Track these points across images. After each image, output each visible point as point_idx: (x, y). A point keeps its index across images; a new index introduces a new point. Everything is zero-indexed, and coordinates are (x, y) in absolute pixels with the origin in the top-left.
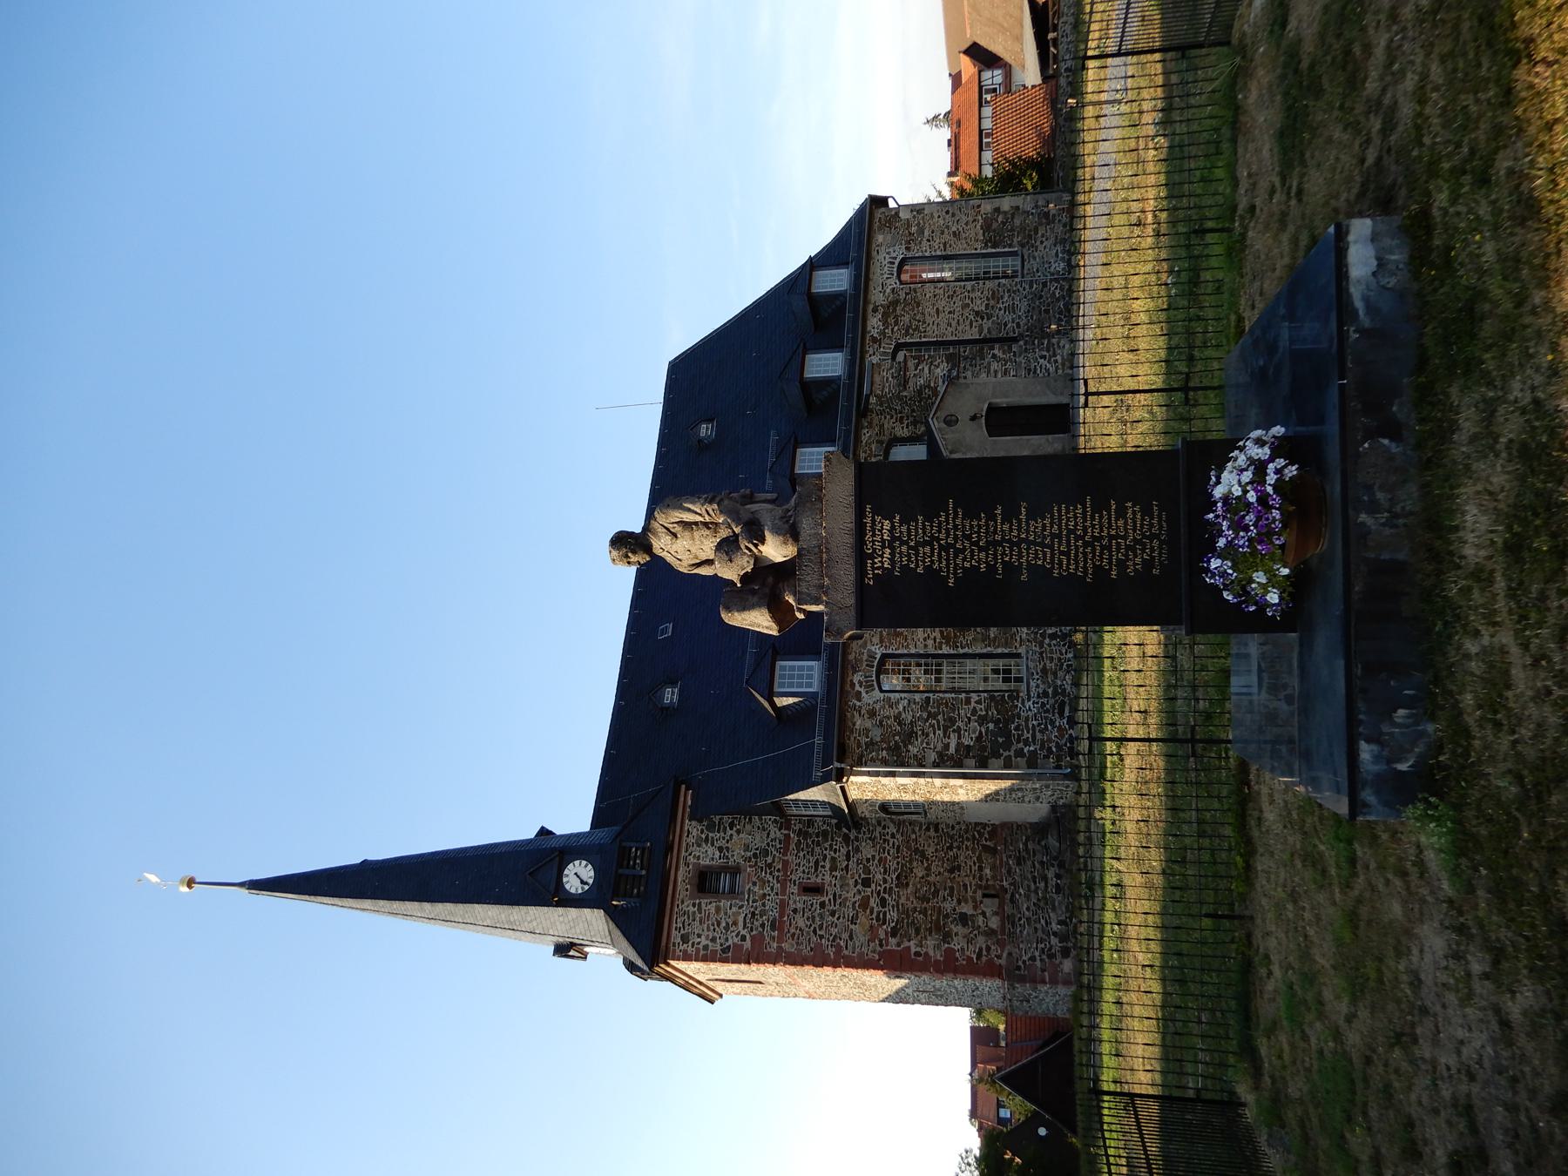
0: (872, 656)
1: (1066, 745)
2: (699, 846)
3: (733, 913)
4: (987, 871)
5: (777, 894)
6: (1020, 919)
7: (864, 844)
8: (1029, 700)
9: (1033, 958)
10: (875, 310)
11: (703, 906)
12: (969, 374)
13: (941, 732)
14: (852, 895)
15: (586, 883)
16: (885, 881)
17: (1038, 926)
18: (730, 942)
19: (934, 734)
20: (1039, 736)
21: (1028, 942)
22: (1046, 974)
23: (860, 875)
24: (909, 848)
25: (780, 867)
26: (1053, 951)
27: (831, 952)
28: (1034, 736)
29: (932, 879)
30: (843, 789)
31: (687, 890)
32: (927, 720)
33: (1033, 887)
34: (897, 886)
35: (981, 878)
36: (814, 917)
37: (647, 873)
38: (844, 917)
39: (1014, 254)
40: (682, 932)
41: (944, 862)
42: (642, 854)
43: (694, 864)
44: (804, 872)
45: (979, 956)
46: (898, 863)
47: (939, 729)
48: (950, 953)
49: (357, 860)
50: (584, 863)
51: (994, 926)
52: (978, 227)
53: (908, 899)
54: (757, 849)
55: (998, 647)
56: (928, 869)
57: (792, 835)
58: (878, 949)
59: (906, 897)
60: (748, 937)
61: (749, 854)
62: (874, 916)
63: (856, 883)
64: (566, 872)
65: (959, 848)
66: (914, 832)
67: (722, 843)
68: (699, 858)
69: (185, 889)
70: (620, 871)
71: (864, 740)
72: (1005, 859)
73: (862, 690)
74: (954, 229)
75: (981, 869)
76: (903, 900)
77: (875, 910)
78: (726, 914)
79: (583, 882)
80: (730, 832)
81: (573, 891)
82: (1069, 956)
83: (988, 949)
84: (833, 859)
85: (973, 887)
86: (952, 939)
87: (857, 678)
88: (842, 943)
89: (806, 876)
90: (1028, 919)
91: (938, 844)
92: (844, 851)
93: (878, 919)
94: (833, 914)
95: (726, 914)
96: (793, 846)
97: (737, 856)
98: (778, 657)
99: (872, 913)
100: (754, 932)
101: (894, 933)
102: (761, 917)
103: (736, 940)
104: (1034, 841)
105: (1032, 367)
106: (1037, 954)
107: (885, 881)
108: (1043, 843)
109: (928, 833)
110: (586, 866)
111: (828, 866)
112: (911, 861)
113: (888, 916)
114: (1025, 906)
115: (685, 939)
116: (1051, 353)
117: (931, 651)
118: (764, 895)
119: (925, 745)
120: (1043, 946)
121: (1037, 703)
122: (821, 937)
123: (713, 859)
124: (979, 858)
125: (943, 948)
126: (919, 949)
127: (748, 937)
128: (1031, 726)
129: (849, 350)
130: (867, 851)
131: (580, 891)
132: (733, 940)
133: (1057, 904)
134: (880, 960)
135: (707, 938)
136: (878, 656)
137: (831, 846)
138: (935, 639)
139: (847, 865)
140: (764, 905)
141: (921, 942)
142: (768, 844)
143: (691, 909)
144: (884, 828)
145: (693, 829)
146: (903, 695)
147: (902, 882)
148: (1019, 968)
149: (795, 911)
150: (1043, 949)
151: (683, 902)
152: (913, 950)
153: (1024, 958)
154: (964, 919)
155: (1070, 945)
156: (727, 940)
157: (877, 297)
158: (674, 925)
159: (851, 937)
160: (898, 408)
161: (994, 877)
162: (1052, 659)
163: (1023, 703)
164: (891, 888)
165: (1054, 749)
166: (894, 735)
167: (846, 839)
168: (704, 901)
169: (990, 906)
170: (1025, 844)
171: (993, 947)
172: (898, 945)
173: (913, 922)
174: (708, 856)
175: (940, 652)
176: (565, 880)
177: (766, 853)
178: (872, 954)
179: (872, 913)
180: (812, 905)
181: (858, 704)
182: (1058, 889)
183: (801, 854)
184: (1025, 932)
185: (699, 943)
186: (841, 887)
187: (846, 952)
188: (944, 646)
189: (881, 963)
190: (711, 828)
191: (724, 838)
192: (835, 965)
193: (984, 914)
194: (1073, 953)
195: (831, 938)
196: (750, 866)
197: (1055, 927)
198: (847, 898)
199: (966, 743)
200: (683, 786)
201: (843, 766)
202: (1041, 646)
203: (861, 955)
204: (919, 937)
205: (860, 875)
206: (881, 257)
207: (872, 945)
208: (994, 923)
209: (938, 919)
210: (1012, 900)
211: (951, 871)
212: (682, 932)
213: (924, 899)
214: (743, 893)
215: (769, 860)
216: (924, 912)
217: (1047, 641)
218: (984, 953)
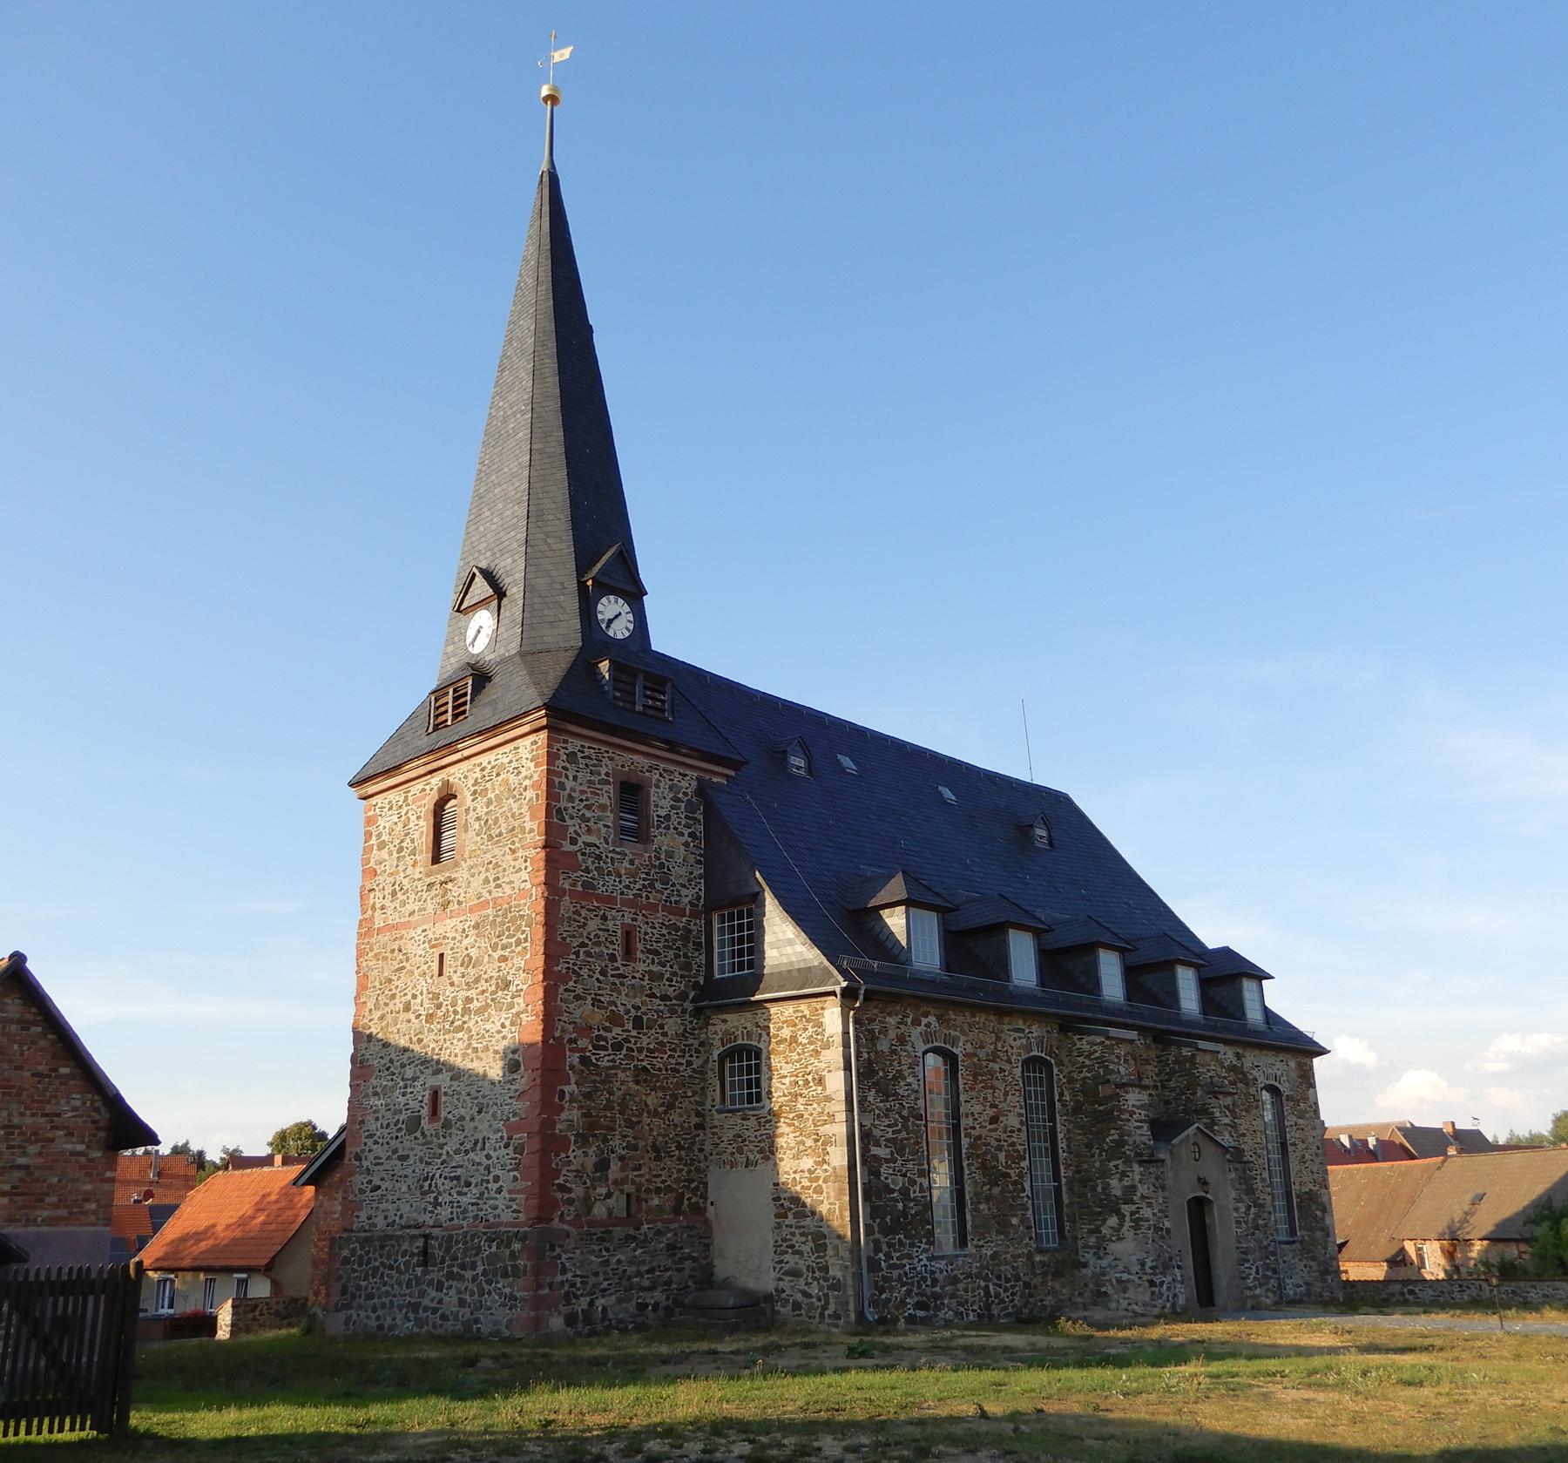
2: (671, 788)
3: (599, 830)
4: (656, 1202)
5: (622, 893)
6: (607, 1250)
7: (679, 1021)
9: (564, 1271)
10: (1238, 1056)
11: (606, 788)
12: (1233, 1175)
13: (889, 1135)
14: (624, 1001)
15: (608, 626)
16: (640, 1050)
17: (601, 1278)
18: (569, 822)
19: (888, 1126)
20: (896, 1273)
22: (547, 1291)
24: (677, 1086)
25: (652, 901)
28: (895, 1267)
29: (646, 1119)
30: (833, 993)
31: (623, 766)
33: (644, 1268)
35: (648, 1191)
36: (598, 944)
37: (639, 713)
38: (599, 988)
39: (1292, 1232)
40: (579, 755)
41: (664, 1136)
42: (656, 709)
43: (650, 779)
44: (646, 934)
45: (562, 1188)
46: (660, 1070)
47: (894, 1133)
48: (563, 1144)
50: (631, 627)
51: (595, 1211)
52: (1311, 1186)
53: (623, 1083)
55: (972, 1216)
56: (656, 1114)
57: (684, 919)
58: (567, 1037)
60: (576, 848)
61: (663, 856)
62: (602, 1032)
63: (637, 1008)
65: (680, 1159)
66: (694, 1093)
67: (674, 821)
68: (657, 786)
69: (545, 91)
71: (877, 1028)
72: (672, 1227)
73: (922, 1028)
74: (1307, 1156)
75: (658, 1190)
76: (621, 1075)
77: (608, 1035)
79: (610, 621)
82: (567, 1326)
83: (570, 1202)
84: (661, 975)
85: (638, 1180)
86: (579, 1148)
87: (931, 1019)
88: (571, 984)
92: (670, 992)
96: (673, 919)
97: (664, 840)
98: (940, 915)
99: (605, 1029)
100: (580, 858)
101: (584, 1061)
103: (571, 830)
104: (693, 1269)
105: (1249, 1257)
107: (640, 1050)
109: (693, 1113)
110: (627, 628)
111: (655, 968)
112: (663, 1088)
113: (603, 1053)
114: (623, 1257)
115: (572, 757)
116: (1261, 1281)
120: (578, 1285)
122: (577, 954)
123: (656, 806)
124: (669, 1189)
125: (569, 1133)
126: (567, 1097)
127: (576, 848)
128: (904, 1262)
129: (1203, 1022)
130: (672, 1026)
131: (600, 617)
132: (572, 825)
133: (625, 1305)
135: (573, 790)
136: (954, 1050)
138: (974, 1128)
140: (609, 874)
141: (576, 1101)
143: (603, 770)
144: (698, 1051)
145: (688, 784)
146: (921, 1083)
147: (641, 1075)
148: (552, 1248)
149: (604, 918)
151: (611, 759)
152: (566, 1089)
153: (564, 1256)
154: (602, 1165)
156: (572, 818)
157: (1250, 1059)
158: (587, 745)
159: (577, 998)
160: (1172, 1084)
161: (650, 1211)
163: (925, 1251)
166: (883, 1070)
167: (682, 997)
169: (618, 1203)
170: (690, 1258)
171: (572, 1209)
172: (572, 1067)
173: (597, 1089)
174: (660, 800)
175: (963, 1136)
178: (563, 1029)
179: (605, 1029)
180: (612, 942)
182: (642, 1307)
184: (593, 1258)
185: (567, 777)
186: (633, 985)
187: (561, 990)
188: (968, 1139)
189: (551, 1041)
190: (691, 808)
191: (679, 823)
193: (609, 1195)
194: (571, 1332)
195: (576, 968)
196: (650, 857)
197: (600, 1302)
199: (882, 1170)
204: (580, 1098)
206: (1279, 1065)
207: (570, 1027)
208: (599, 1211)
211: (655, 1148)
212: (579, 755)
215: (658, 885)
216: (608, 1106)
217: (983, 1284)
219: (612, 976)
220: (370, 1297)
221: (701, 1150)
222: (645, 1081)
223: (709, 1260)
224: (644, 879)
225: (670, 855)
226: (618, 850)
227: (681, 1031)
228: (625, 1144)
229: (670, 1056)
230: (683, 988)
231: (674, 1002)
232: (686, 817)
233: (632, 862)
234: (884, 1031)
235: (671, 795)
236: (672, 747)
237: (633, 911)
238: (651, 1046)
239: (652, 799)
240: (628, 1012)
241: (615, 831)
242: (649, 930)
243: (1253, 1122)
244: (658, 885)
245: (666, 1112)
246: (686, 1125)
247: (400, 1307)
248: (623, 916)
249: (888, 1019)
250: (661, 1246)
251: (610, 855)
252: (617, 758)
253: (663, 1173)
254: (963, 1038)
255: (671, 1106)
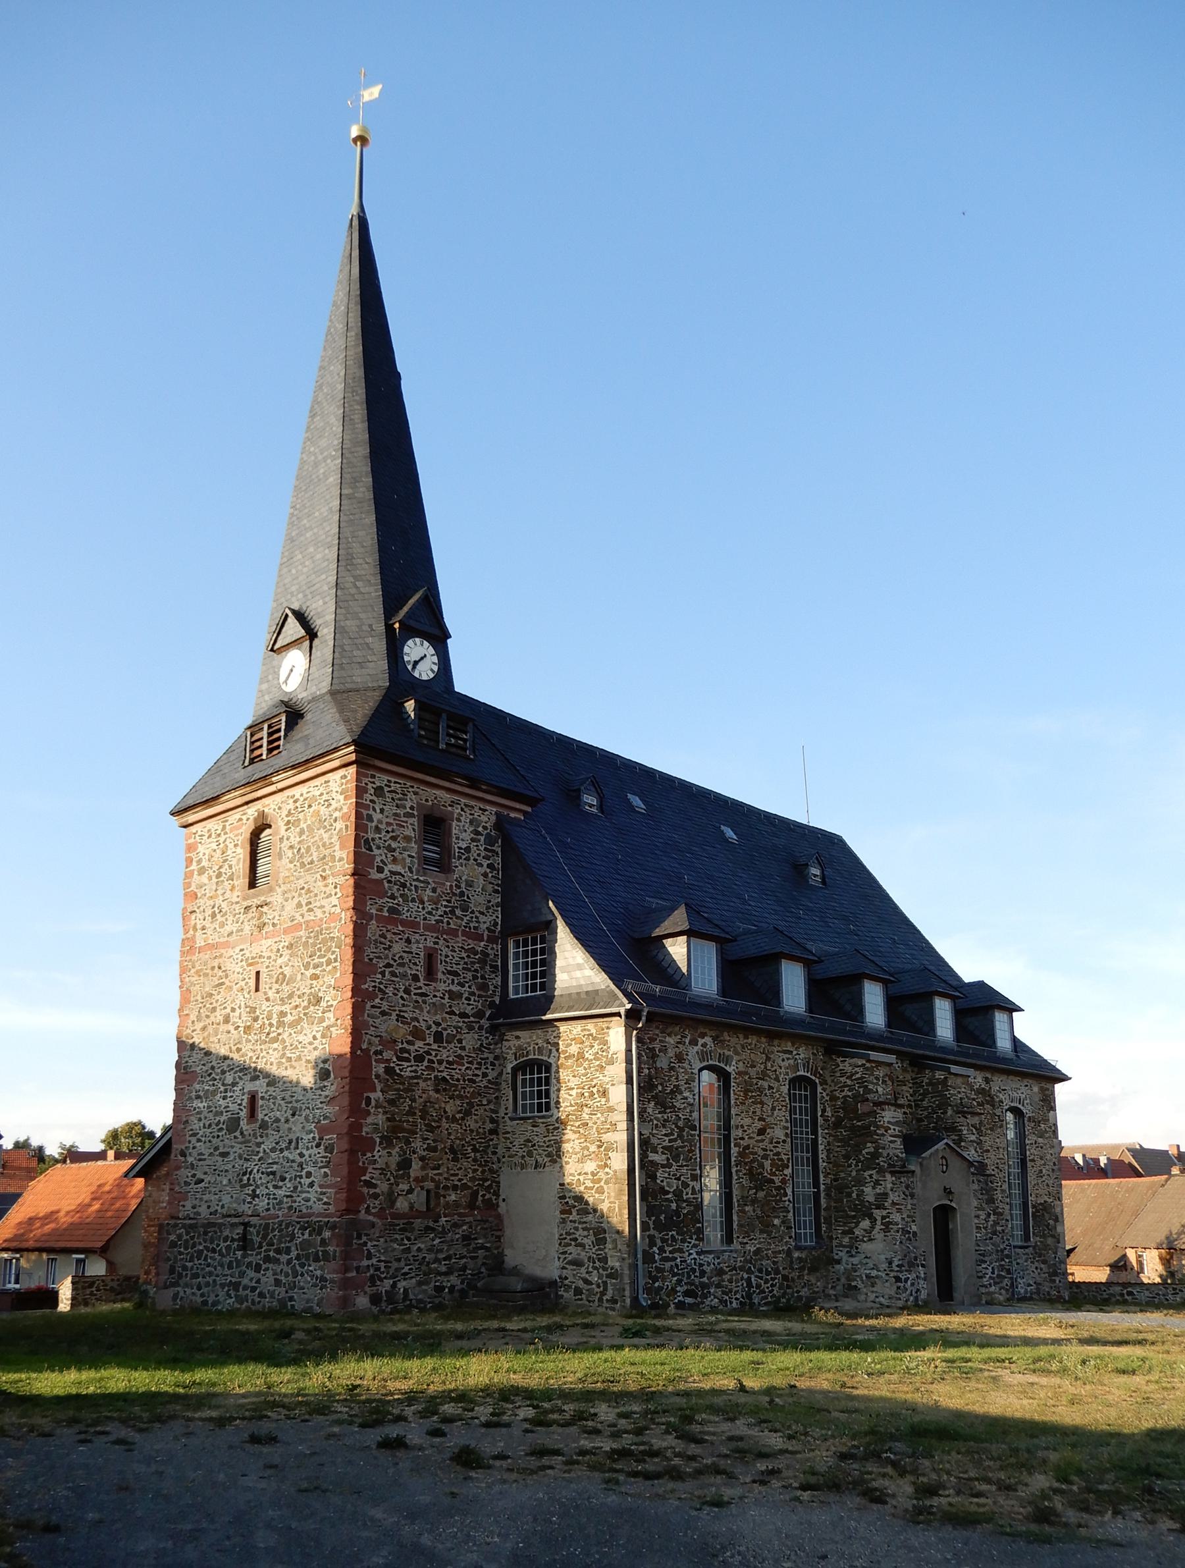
0: (728, 1061)
1: (660, 1299)
2: (471, 822)
3: (404, 859)
4: (453, 1197)
5: (425, 919)
6: (409, 1239)
8: (698, 1253)
10: (987, 1081)
11: (411, 820)
13: (666, 1143)
14: (426, 1018)
15: (414, 667)
16: (440, 1062)
17: (402, 1263)
18: (376, 852)
19: (666, 1135)
20: (668, 1265)
21: (386, 1250)
22: (354, 1274)
23: (445, 1029)
24: (473, 1095)
26: (378, 1283)
27: (367, 986)
29: (445, 1124)
30: (618, 1014)
31: (427, 800)
32: (677, 1126)
33: (441, 1256)
34: (436, 1077)
36: (402, 965)
37: (442, 750)
38: (403, 1005)
39: (1026, 1237)
40: (386, 789)
43: (452, 813)
44: (447, 956)
45: (368, 1184)
46: (458, 1080)
47: (670, 1141)
48: (368, 1145)
49: (401, 367)
50: (436, 668)
51: (398, 1204)
52: (1046, 1198)
53: (424, 1091)
54: (468, 898)
58: (373, 1050)
59: (425, 1089)
60: (382, 876)
61: (463, 885)
62: (405, 1045)
63: (438, 1024)
64: (426, 644)
65: (475, 1160)
66: (489, 1102)
67: (474, 853)
68: (459, 820)
69: (355, 132)
70: (444, 716)
71: (657, 1046)
75: (455, 1188)
76: (422, 1084)
77: (411, 1048)
78: (405, 849)
79: (416, 663)
80: (485, 865)
81: (406, 650)
83: (375, 1196)
84: (460, 995)
85: (437, 1178)
86: (384, 1149)
87: (708, 1040)
88: (377, 1001)
89: (443, 959)
90: (408, 1250)
91: (478, 1133)
92: (469, 1010)
93: (403, 1050)
94: (407, 991)
95: (405, 849)
96: (472, 944)
97: (462, 870)
99: (409, 1042)
100: (386, 885)
101: (389, 1071)
102: (402, 896)
103: (378, 859)
104: (485, 1257)
106: (374, 1261)
108: (483, 1270)
110: (432, 670)
111: (455, 988)
112: (460, 1097)
113: (406, 1064)
114: (422, 1246)
115: (379, 791)
117: (734, 1133)
118: (422, 902)
119: (655, 1122)
121: (695, 1263)
122: (383, 973)
124: (465, 1187)
125: (374, 1136)
126: (373, 1103)
127: (382, 876)
130: (470, 1040)
131: (406, 658)
132: (379, 855)
133: (424, 1287)
134: (361, 1049)
135: (380, 822)
136: (727, 1068)
137: (473, 994)
138: (742, 1139)
139: (455, 1015)
140: (413, 900)
141: (381, 1107)
142: (473, 912)
143: (408, 804)
144: (493, 1064)
145: (487, 818)
147: (441, 1084)
149: (408, 941)
150: (378, 1269)
151: (416, 793)
152: (372, 1095)
153: (369, 1244)
154: (405, 1164)
155: (384, 1305)
156: (378, 848)
157: (998, 1083)
158: (393, 780)
159: (383, 1013)
160: (925, 1103)
162: (730, 1281)
163: (695, 1246)
164: (433, 1069)
165: (657, 1284)
167: (479, 1014)
168: (414, 820)
169: (418, 1199)
170: (482, 1247)
171: (377, 1202)
172: (378, 1076)
173: (401, 1097)
174: (461, 834)
176: (418, 640)
177: (465, 909)
179: (409, 1042)
180: (415, 964)
181: (687, 1041)
183: (464, 955)
184: (395, 1246)
185: (374, 810)
188: (737, 1149)
189: (359, 1052)
190: (490, 841)
192: (356, 990)
193: (410, 1191)
194: (375, 1309)
195: (382, 986)
196: (451, 886)
197: (402, 1285)
198: (422, 1010)
199: (658, 1175)
200: (529, 809)
201: (644, 1018)
202: (742, 1269)
203: (366, 1025)
204: (386, 1104)
205: (445, 1029)
206: (1023, 1089)
208: (402, 1205)
209: (403, 1130)
210: (428, 1229)
212: (386, 789)
213: (424, 1113)
214: (425, 874)
215: (458, 912)
216: (411, 1113)
217: (746, 1276)
218: (372, 1191)
219: (415, 994)
220: (195, 1276)
221: (494, 1153)
222: (445, 1090)
223: (500, 1250)
224: (446, 906)
225: (469, 884)
226: (421, 878)
227: (478, 1046)
228: (425, 1146)
229: (467, 1068)
230: (480, 1007)
231: (472, 1019)
232: (486, 849)
233: (434, 890)
234: (664, 1050)
235: (471, 829)
236: (474, 783)
237: (435, 935)
238: (451, 1059)
239: (454, 831)
240: (429, 1028)
241: (419, 861)
242: (450, 953)
243: (997, 1140)
244: (458, 912)
245: (463, 1119)
246: (481, 1130)
247: (223, 1286)
248: (426, 939)
249: (668, 1039)
250: (457, 1236)
251: (414, 883)
252: (421, 792)
253: (459, 1172)
254: (736, 1058)
255: (467, 1113)
